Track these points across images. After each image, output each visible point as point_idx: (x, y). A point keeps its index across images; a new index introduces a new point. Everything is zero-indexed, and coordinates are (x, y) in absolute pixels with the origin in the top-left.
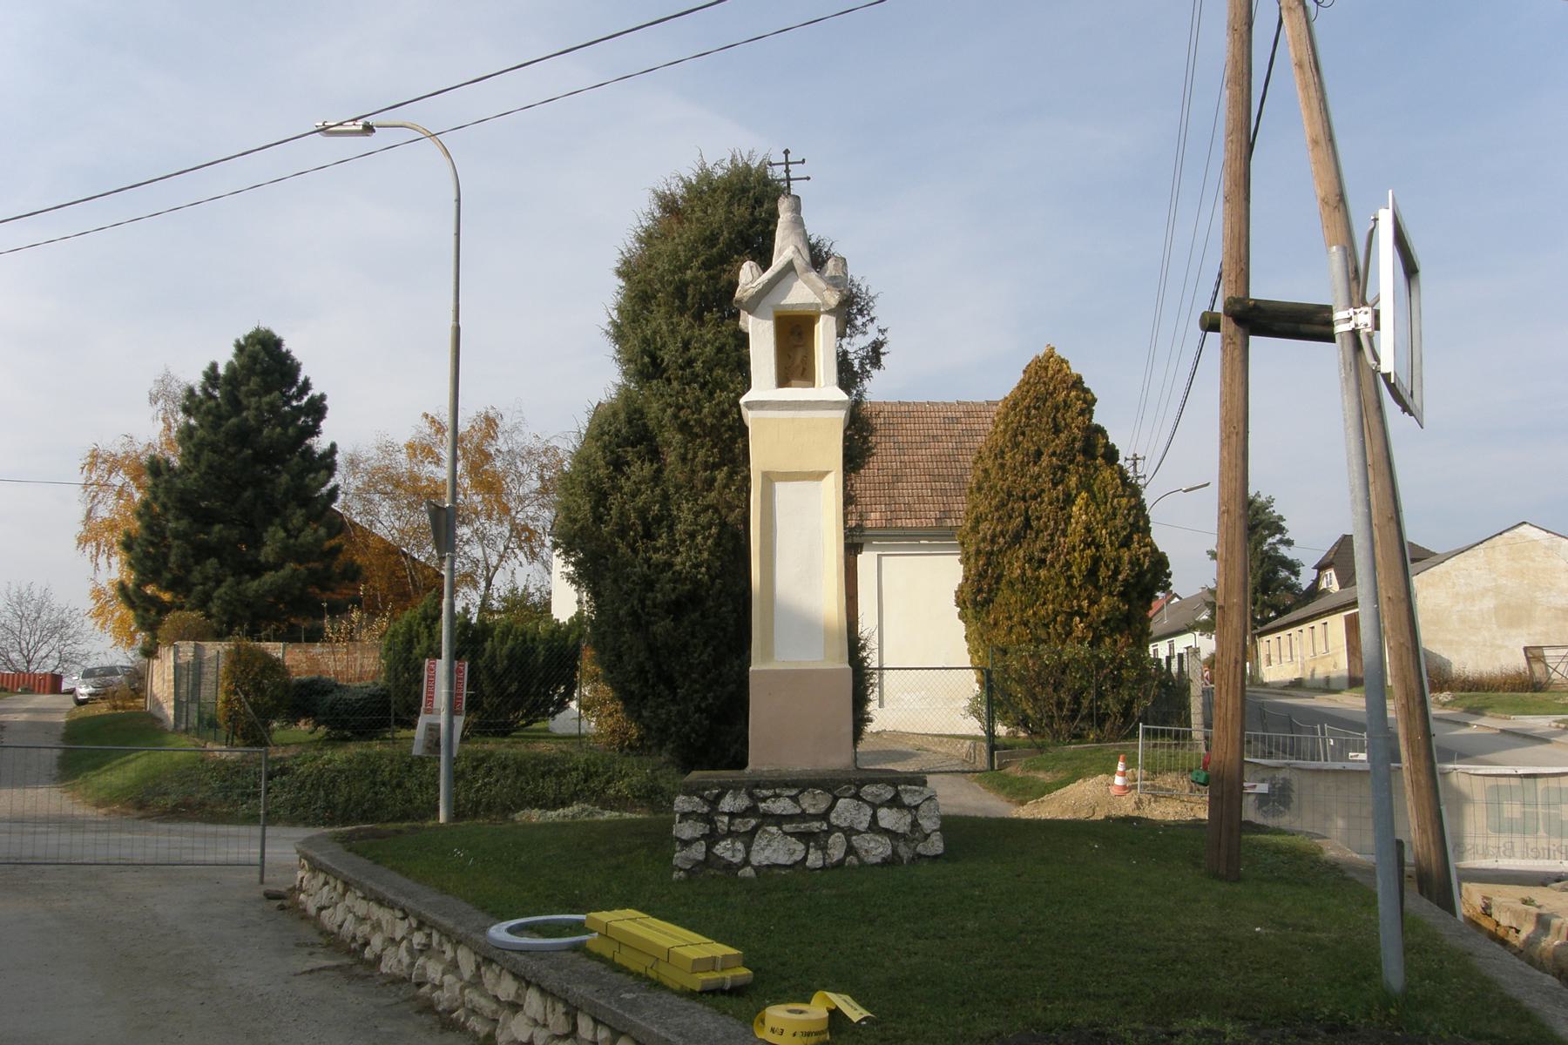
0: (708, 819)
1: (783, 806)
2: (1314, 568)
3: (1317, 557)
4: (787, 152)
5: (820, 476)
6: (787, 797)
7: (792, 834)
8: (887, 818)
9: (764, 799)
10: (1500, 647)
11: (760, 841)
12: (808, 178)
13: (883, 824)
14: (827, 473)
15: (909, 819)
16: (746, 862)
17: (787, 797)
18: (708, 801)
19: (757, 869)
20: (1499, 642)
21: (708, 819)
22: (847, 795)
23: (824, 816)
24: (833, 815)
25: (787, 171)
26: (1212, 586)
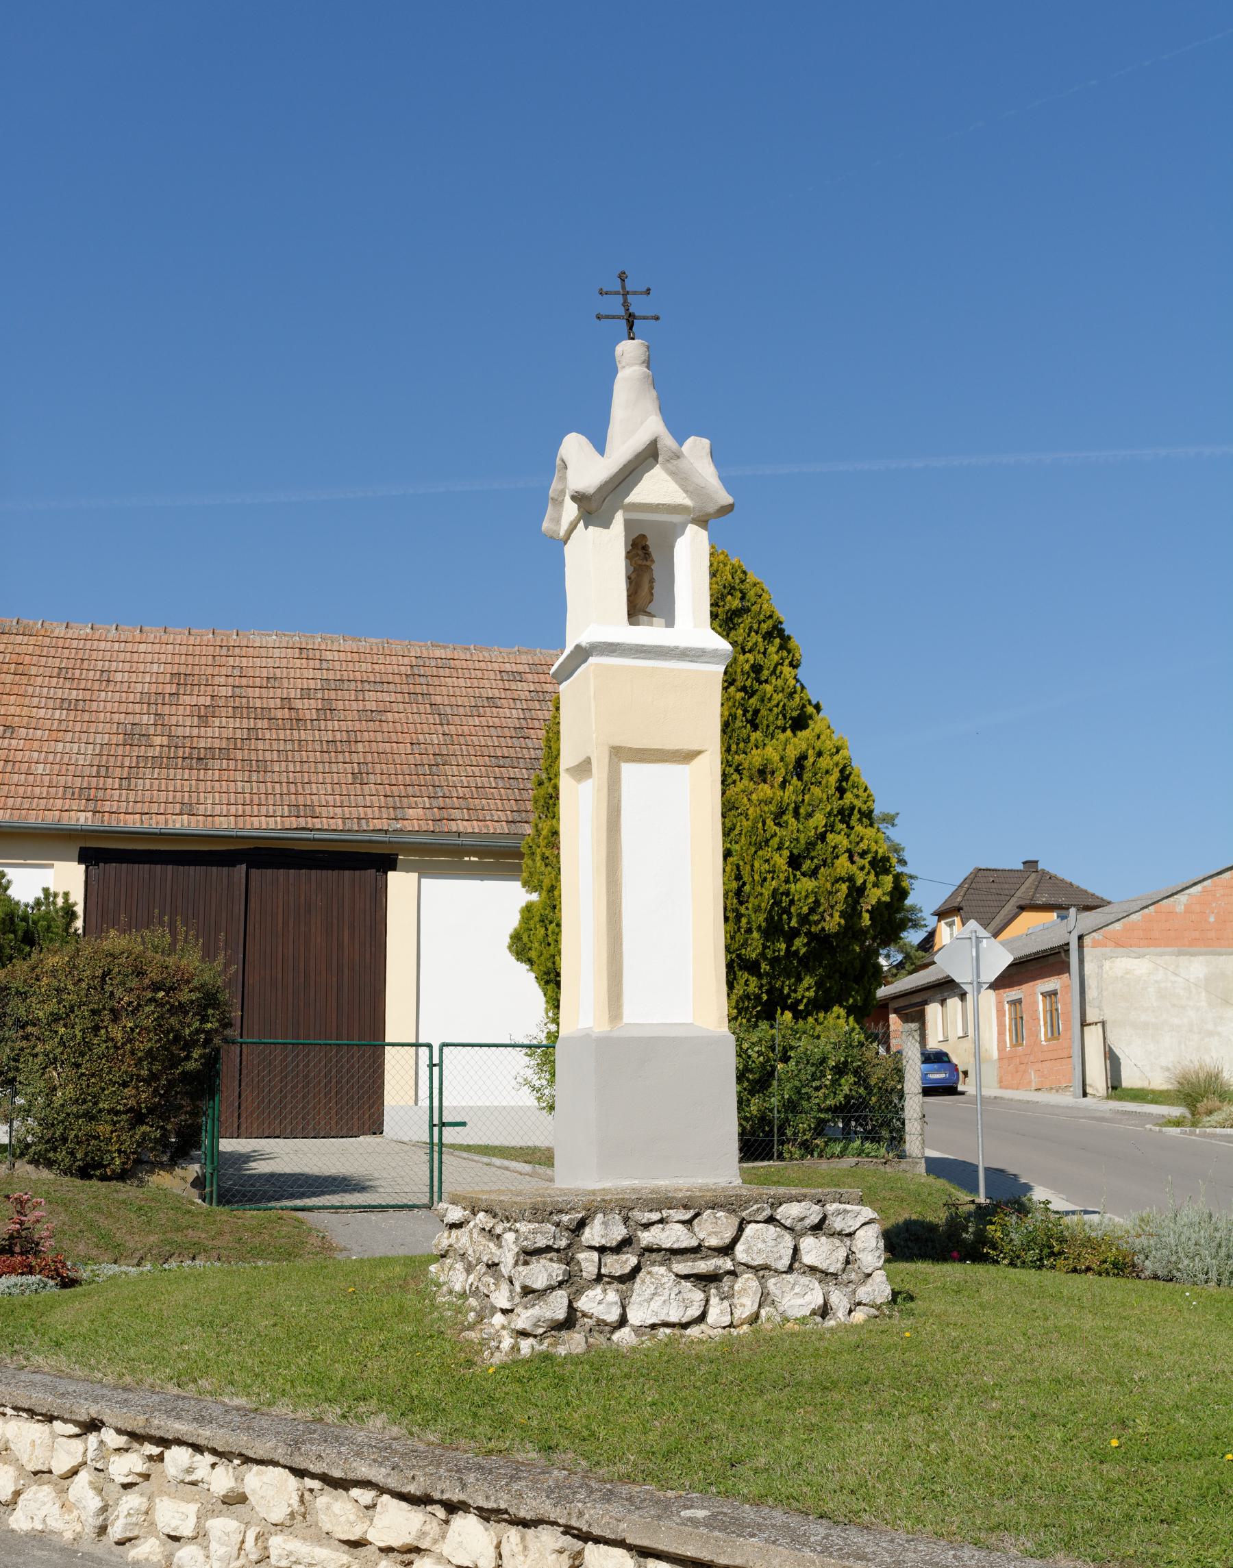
0: (567, 1256)
1: (673, 1235)
2: (932, 914)
3: (936, 905)
4: (622, 277)
5: (687, 756)
6: (678, 1222)
7: (686, 1277)
8: (815, 1251)
9: (647, 1226)
10: (1211, 1034)
11: (643, 1287)
12: (657, 318)
13: (808, 1259)
14: (699, 753)
15: (842, 1254)
16: (623, 1321)
17: (678, 1222)
18: (568, 1229)
19: (638, 1330)
20: (1210, 1027)
21: (567, 1256)
22: (760, 1218)
23: (727, 1250)
24: (739, 1247)
25: (626, 304)
26: (9, 892)
